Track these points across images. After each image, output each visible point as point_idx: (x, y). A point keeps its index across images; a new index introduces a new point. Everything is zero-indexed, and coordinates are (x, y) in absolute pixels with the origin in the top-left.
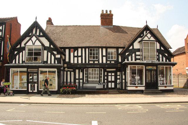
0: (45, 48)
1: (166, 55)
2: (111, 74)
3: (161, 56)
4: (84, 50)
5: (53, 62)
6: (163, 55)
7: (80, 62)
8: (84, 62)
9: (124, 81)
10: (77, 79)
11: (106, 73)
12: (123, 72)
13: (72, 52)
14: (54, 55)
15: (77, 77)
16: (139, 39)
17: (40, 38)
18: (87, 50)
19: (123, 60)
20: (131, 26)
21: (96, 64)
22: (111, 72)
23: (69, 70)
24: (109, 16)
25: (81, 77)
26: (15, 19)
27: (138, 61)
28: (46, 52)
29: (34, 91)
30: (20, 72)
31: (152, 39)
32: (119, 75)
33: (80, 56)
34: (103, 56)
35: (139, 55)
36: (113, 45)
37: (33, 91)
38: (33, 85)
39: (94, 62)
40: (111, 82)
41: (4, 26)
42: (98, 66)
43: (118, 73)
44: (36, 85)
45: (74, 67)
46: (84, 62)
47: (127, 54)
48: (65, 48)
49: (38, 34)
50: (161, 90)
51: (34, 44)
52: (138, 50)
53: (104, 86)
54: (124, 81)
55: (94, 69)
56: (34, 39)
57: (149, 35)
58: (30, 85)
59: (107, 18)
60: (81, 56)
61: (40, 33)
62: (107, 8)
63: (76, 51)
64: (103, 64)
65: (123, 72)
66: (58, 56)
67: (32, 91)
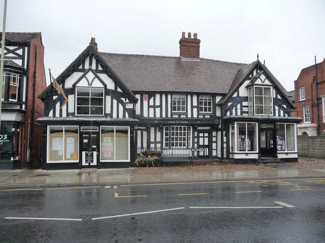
0: (108, 92)
1: (285, 106)
2: (204, 135)
3: (277, 108)
4: (164, 96)
5: (121, 116)
6: (280, 107)
7: (158, 115)
8: (164, 116)
9: (225, 145)
10: (153, 143)
11: (196, 133)
12: (224, 132)
13: (145, 100)
14: (124, 105)
15: (152, 140)
16: (247, 82)
17: (99, 75)
18: (169, 97)
19: (224, 113)
20: (120, 53)
21: (182, 120)
22: (204, 132)
23: (139, 128)
24: (194, 43)
25: (158, 139)
26: (37, 36)
27: (245, 115)
28: (109, 98)
29: (91, 164)
30: (116, 132)
31: (267, 82)
32: (215, 137)
33: (158, 107)
34: (192, 107)
35: (247, 107)
36: (208, 91)
37: (89, 164)
38: (89, 153)
39: (180, 116)
40: (204, 146)
41: (26, 49)
42: (187, 122)
43: (214, 134)
44: (95, 153)
45: (148, 124)
46: (164, 116)
47: (229, 104)
48: (136, 92)
49: (94, 67)
50: (282, 159)
51: (90, 84)
52: (246, 99)
53: (193, 152)
54: (225, 145)
55: (179, 127)
56: (90, 76)
57: (263, 77)
58: (84, 153)
59: (190, 45)
60: (161, 106)
61: (97, 67)
62: (190, 29)
63: (153, 98)
64: (143, 118)
65: (224, 132)
66: (130, 106)
67: (88, 164)
